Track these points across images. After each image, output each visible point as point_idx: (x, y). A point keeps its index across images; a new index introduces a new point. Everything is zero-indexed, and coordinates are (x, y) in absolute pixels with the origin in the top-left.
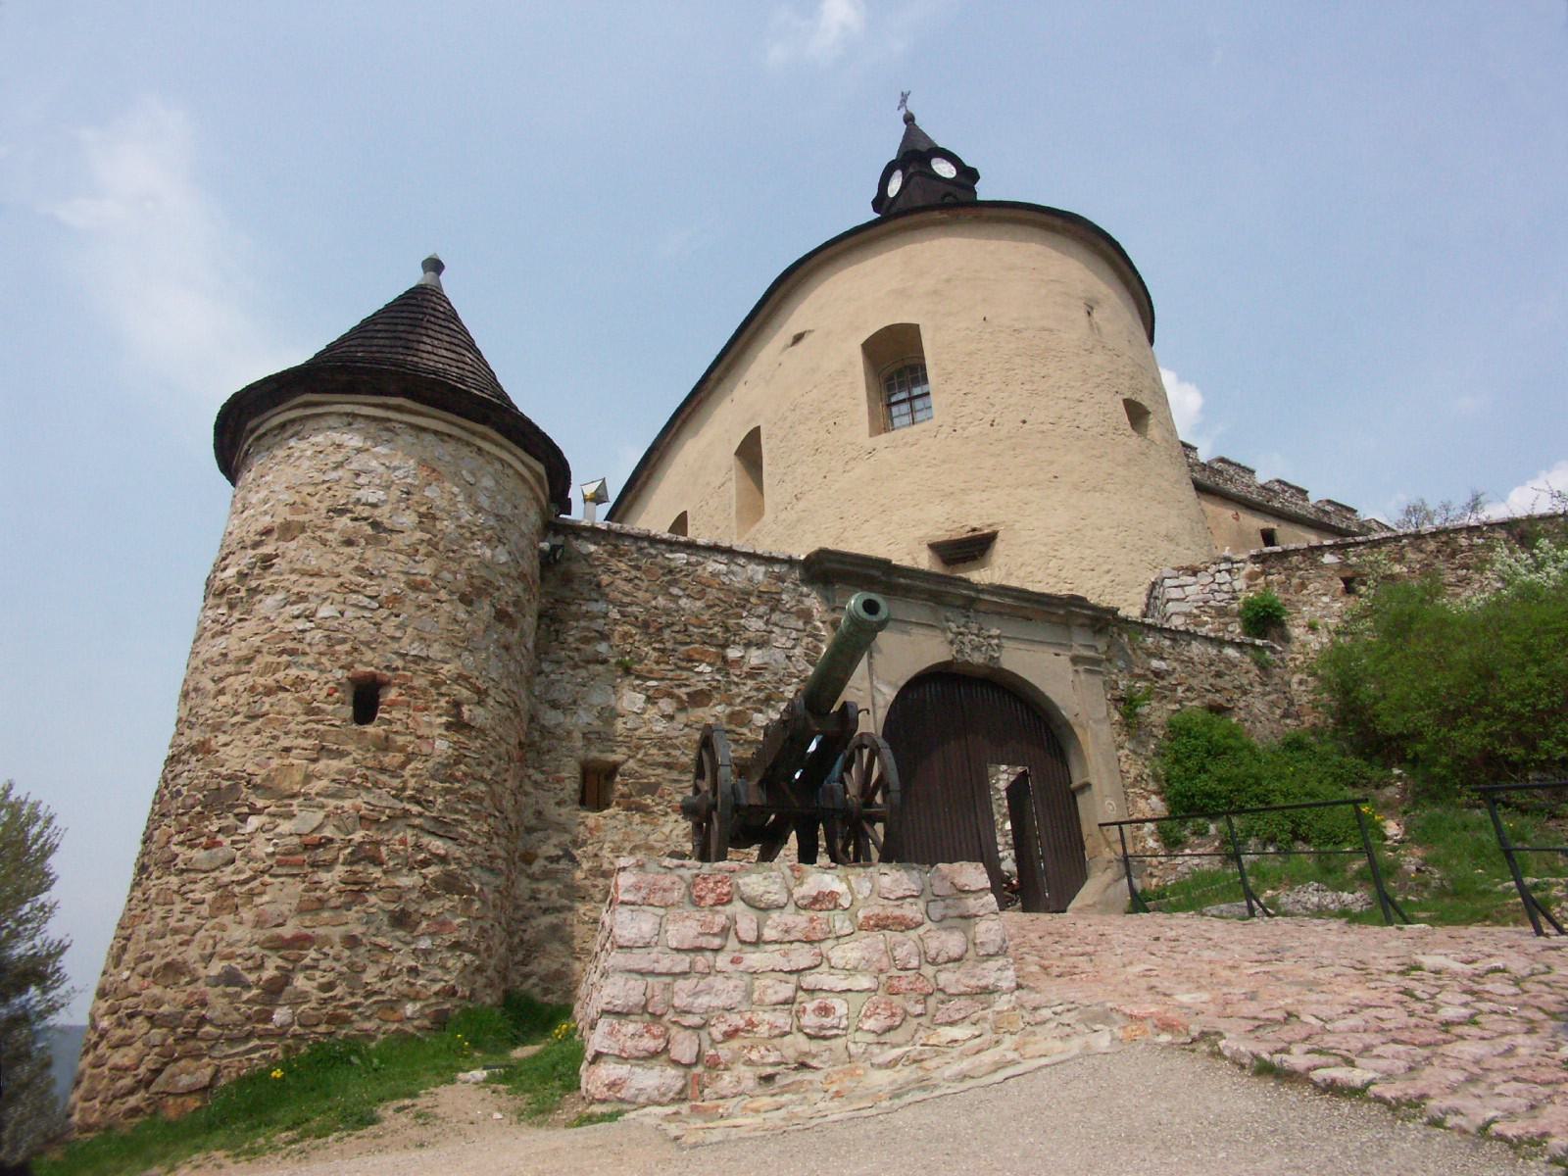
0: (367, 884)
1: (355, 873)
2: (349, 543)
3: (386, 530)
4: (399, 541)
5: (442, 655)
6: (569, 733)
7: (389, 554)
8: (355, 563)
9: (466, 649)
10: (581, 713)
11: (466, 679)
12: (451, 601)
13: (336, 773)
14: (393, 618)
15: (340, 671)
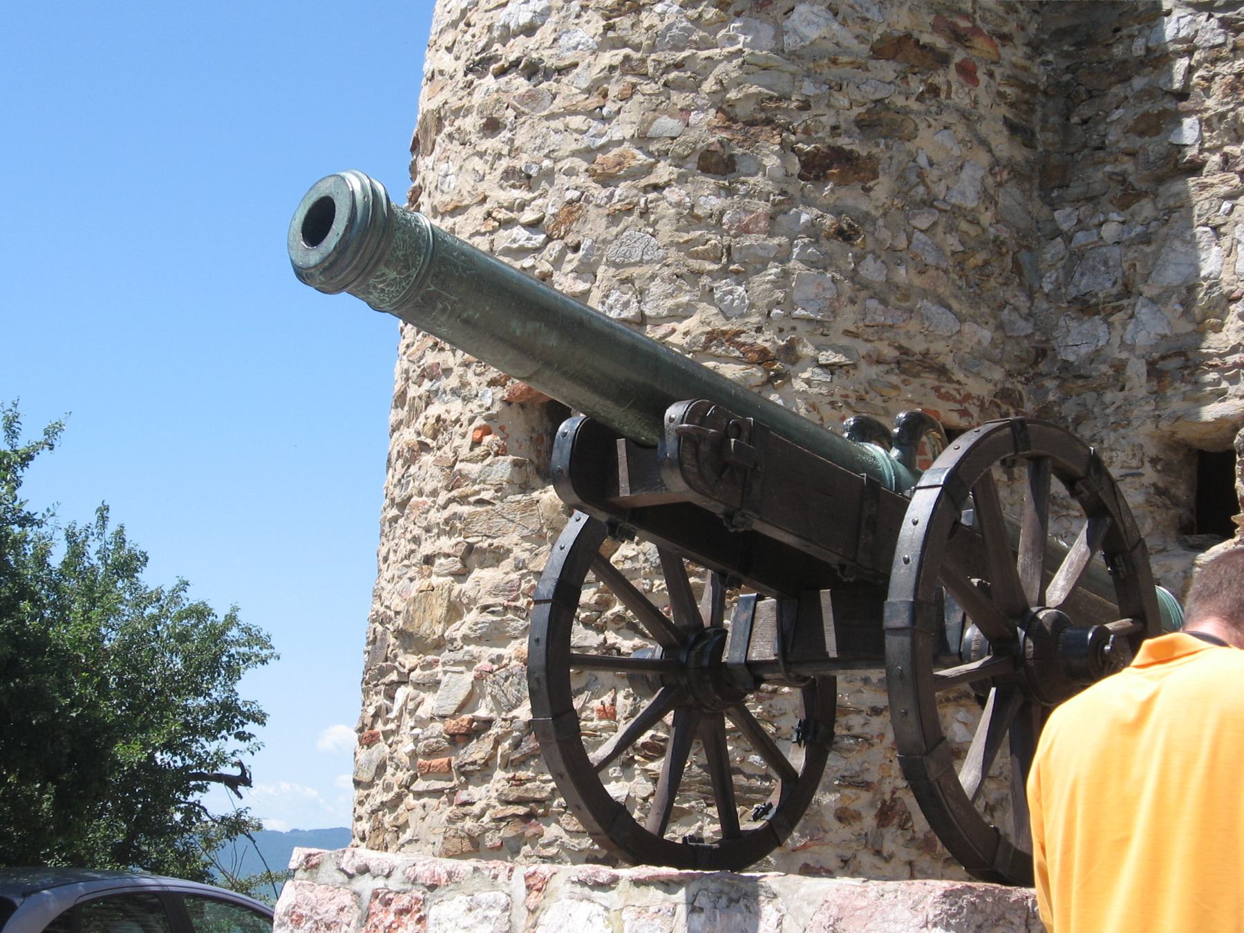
0: (540, 802)
1: (521, 782)
2: (492, 126)
3: (548, 74)
4: (570, 89)
5: (670, 302)
6: (1120, 367)
7: (557, 124)
8: (504, 163)
9: (725, 273)
10: (1144, 313)
11: (730, 338)
12: (682, 180)
13: (489, 593)
14: (570, 256)
15: (490, 391)
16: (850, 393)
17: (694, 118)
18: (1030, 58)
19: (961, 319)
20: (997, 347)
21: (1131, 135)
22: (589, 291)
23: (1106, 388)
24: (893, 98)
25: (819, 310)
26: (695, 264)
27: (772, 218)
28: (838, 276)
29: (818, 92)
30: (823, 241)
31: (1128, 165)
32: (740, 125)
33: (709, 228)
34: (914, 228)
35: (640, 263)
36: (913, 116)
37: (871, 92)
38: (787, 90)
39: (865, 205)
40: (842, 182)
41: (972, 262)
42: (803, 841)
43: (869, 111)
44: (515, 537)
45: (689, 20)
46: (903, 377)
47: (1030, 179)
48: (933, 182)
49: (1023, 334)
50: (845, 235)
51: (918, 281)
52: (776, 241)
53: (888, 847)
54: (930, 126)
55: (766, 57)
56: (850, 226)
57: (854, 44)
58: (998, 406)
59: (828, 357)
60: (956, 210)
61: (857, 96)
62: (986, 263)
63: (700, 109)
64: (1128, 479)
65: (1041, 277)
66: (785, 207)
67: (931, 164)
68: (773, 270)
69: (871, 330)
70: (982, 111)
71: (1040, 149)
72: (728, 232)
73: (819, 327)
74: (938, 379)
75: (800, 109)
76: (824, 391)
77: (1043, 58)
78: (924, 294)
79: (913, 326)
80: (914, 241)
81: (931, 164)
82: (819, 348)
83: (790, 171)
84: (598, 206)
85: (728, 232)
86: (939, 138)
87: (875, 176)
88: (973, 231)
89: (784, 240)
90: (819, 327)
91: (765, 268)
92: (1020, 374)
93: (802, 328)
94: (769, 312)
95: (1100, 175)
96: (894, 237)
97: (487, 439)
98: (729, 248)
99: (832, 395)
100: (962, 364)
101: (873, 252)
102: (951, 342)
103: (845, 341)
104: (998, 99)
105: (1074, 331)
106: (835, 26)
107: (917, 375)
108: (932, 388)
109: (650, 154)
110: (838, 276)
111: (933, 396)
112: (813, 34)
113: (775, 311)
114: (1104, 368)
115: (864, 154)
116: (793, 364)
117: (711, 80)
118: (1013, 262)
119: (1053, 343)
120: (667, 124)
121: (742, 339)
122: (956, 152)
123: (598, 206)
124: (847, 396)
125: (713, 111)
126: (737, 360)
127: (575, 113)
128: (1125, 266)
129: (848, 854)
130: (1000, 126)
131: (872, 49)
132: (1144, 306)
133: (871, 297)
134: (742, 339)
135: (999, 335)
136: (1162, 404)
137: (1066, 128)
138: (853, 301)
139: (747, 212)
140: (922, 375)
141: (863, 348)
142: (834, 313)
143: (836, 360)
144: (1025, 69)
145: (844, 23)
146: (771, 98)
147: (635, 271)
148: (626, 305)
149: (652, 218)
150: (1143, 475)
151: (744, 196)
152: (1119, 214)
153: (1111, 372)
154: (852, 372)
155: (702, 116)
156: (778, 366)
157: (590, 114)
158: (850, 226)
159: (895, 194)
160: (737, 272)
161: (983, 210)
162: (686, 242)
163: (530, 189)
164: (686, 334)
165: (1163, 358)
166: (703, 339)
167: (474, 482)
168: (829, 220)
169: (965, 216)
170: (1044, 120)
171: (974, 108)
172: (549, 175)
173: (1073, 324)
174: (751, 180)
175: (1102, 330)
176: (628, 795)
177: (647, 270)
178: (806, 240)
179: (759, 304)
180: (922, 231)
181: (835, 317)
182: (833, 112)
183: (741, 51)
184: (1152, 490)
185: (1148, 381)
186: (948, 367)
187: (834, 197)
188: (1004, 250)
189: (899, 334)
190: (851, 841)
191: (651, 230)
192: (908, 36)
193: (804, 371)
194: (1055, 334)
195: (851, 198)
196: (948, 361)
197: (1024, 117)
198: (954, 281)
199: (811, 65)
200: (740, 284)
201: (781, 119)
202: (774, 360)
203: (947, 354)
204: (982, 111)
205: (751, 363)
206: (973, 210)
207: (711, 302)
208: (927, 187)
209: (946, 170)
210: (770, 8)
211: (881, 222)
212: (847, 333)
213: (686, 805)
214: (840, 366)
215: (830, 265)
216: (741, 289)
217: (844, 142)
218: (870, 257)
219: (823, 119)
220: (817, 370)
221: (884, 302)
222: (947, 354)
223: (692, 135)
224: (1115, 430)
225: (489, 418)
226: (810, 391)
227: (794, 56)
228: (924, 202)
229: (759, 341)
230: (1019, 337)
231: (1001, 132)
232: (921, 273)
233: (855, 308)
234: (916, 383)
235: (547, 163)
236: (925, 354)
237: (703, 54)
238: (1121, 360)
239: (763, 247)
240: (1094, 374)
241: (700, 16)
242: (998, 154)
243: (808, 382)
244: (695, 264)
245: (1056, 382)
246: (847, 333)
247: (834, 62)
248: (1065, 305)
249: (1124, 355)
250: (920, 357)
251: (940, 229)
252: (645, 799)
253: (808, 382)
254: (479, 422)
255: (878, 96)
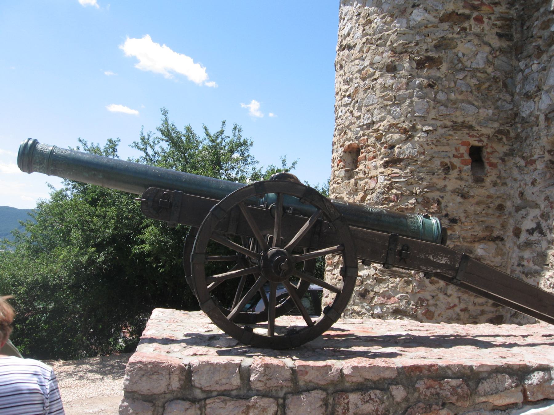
5: (379, 116)
6: (537, 118)
7: (353, 63)
9: (394, 104)
12: (382, 76)
16: (434, 140)
17: (384, 55)
18: (509, 9)
19: (478, 108)
20: (495, 115)
21: (540, 30)
22: (361, 115)
23: (533, 126)
24: (447, 35)
25: (423, 113)
26: (385, 103)
27: (407, 84)
28: (429, 100)
29: (421, 38)
30: (424, 89)
31: (540, 42)
32: (398, 54)
33: (389, 90)
34: (457, 79)
35: (372, 104)
36: (455, 40)
37: (439, 35)
38: (411, 40)
39: (438, 74)
40: (430, 68)
41: (484, 87)
42: (419, 290)
43: (439, 42)
44: (345, 194)
45: (383, 23)
46: (454, 131)
47: (510, 52)
48: (465, 61)
49: (508, 109)
50: (431, 86)
51: (460, 97)
52: (408, 91)
53: (449, 292)
54: (462, 42)
55: (404, 30)
56: (433, 82)
57: (433, 19)
58: (497, 136)
59: (425, 128)
60: (475, 70)
61: (434, 37)
62: (490, 86)
63: (386, 51)
64: (539, 159)
65: (516, 87)
66: (411, 79)
67: (464, 55)
68: (408, 101)
69: (442, 117)
70: (486, 32)
71: (515, 40)
72: (394, 90)
73: (423, 118)
74: (469, 130)
75: (415, 45)
76: (425, 140)
77: (515, 7)
78: (463, 101)
79: (458, 113)
80: (457, 84)
81: (464, 55)
82: (423, 126)
83: (413, 67)
84: (362, 88)
85: (394, 90)
86: (466, 45)
87: (441, 63)
88: (483, 76)
89: (411, 91)
90: (423, 118)
91: (406, 101)
92: (507, 123)
93: (418, 119)
94: (407, 116)
95: (532, 47)
96: (449, 84)
97: (340, 163)
98: (395, 96)
99: (427, 141)
100: (480, 124)
101: (441, 90)
102: (474, 117)
103: (433, 122)
104: (493, 27)
105: (525, 106)
106: (426, 15)
107: (460, 130)
108: (467, 134)
109: (374, 69)
110: (429, 100)
111: (467, 136)
112: (419, 19)
113: (409, 115)
114: (533, 118)
115: (437, 57)
116: (415, 132)
117: (389, 41)
118: (503, 84)
119: (519, 111)
120: (378, 58)
121: (399, 126)
122: (474, 49)
123: (362, 88)
124: (433, 141)
125: (390, 51)
126: (398, 133)
127: (356, 59)
128: (538, 79)
129: (434, 294)
130: (494, 36)
131: (439, 20)
132: (544, 94)
133: (441, 106)
134: (399, 126)
135: (496, 111)
136: (549, 130)
137: (522, 32)
138: (434, 108)
139: (400, 83)
140: (462, 130)
141: (439, 123)
142: (428, 113)
143: (429, 129)
144: (507, 13)
145: (429, 13)
146: (406, 44)
147: (370, 107)
148: (369, 118)
149: (375, 89)
150: (544, 157)
151: (399, 78)
152: (537, 61)
153: (535, 120)
154: (434, 132)
155: (387, 54)
156: (410, 133)
157: (359, 59)
158: (433, 82)
159: (449, 69)
160: (397, 104)
161: (488, 67)
162: (383, 96)
163: (348, 85)
164: (383, 126)
165: (549, 113)
166: (388, 127)
167: (337, 177)
168: (426, 82)
169: (479, 71)
170: (516, 30)
171: (483, 32)
172: (351, 80)
173: (525, 103)
174: (401, 72)
175: (533, 104)
176: (368, 274)
177: (373, 107)
178: (418, 90)
179: (404, 113)
180: (461, 79)
181: (428, 114)
182: (426, 44)
183: (397, 30)
184: (549, 162)
185: (545, 122)
186: (473, 125)
187: (427, 73)
188: (498, 80)
189: (452, 117)
190: (435, 290)
191: (374, 93)
192: (453, 12)
193: (419, 134)
194: (520, 108)
195: (434, 73)
196: (474, 124)
197: (506, 30)
198: (475, 95)
199: (418, 30)
200: (398, 108)
201: (409, 50)
202: (408, 132)
203: (473, 121)
204: (486, 32)
205: (401, 133)
206: (483, 68)
207: (391, 115)
208: (463, 64)
209: (470, 56)
210: (405, 13)
211: (444, 79)
212: (433, 119)
213: (384, 278)
214: (430, 131)
215: (426, 97)
216: (398, 109)
217: (430, 54)
218: (440, 92)
219: (423, 47)
220: (423, 133)
221: (446, 106)
222: (473, 121)
223: (384, 60)
224: (536, 141)
225: (341, 157)
226: (420, 140)
227: (414, 28)
228: (461, 69)
229: (404, 126)
230: (506, 110)
231: (495, 38)
232: (461, 94)
233: (435, 110)
234: (459, 133)
235: (351, 76)
236: (464, 122)
237: (386, 33)
238: (538, 115)
239: (404, 94)
240: (530, 121)
241: (386, 21)
242: (493, 46)
243: (419, 137)
244: (385, 103)
245: (520, 125)
246: (433, 119)
247: (426, 27)
248: (523, 96)
249: (538, 113)
250: (461, 124)
251: (468, 78)
252: (373, 275)
253: (419, 137)
254: (339, 159)
255: (442, 36)
